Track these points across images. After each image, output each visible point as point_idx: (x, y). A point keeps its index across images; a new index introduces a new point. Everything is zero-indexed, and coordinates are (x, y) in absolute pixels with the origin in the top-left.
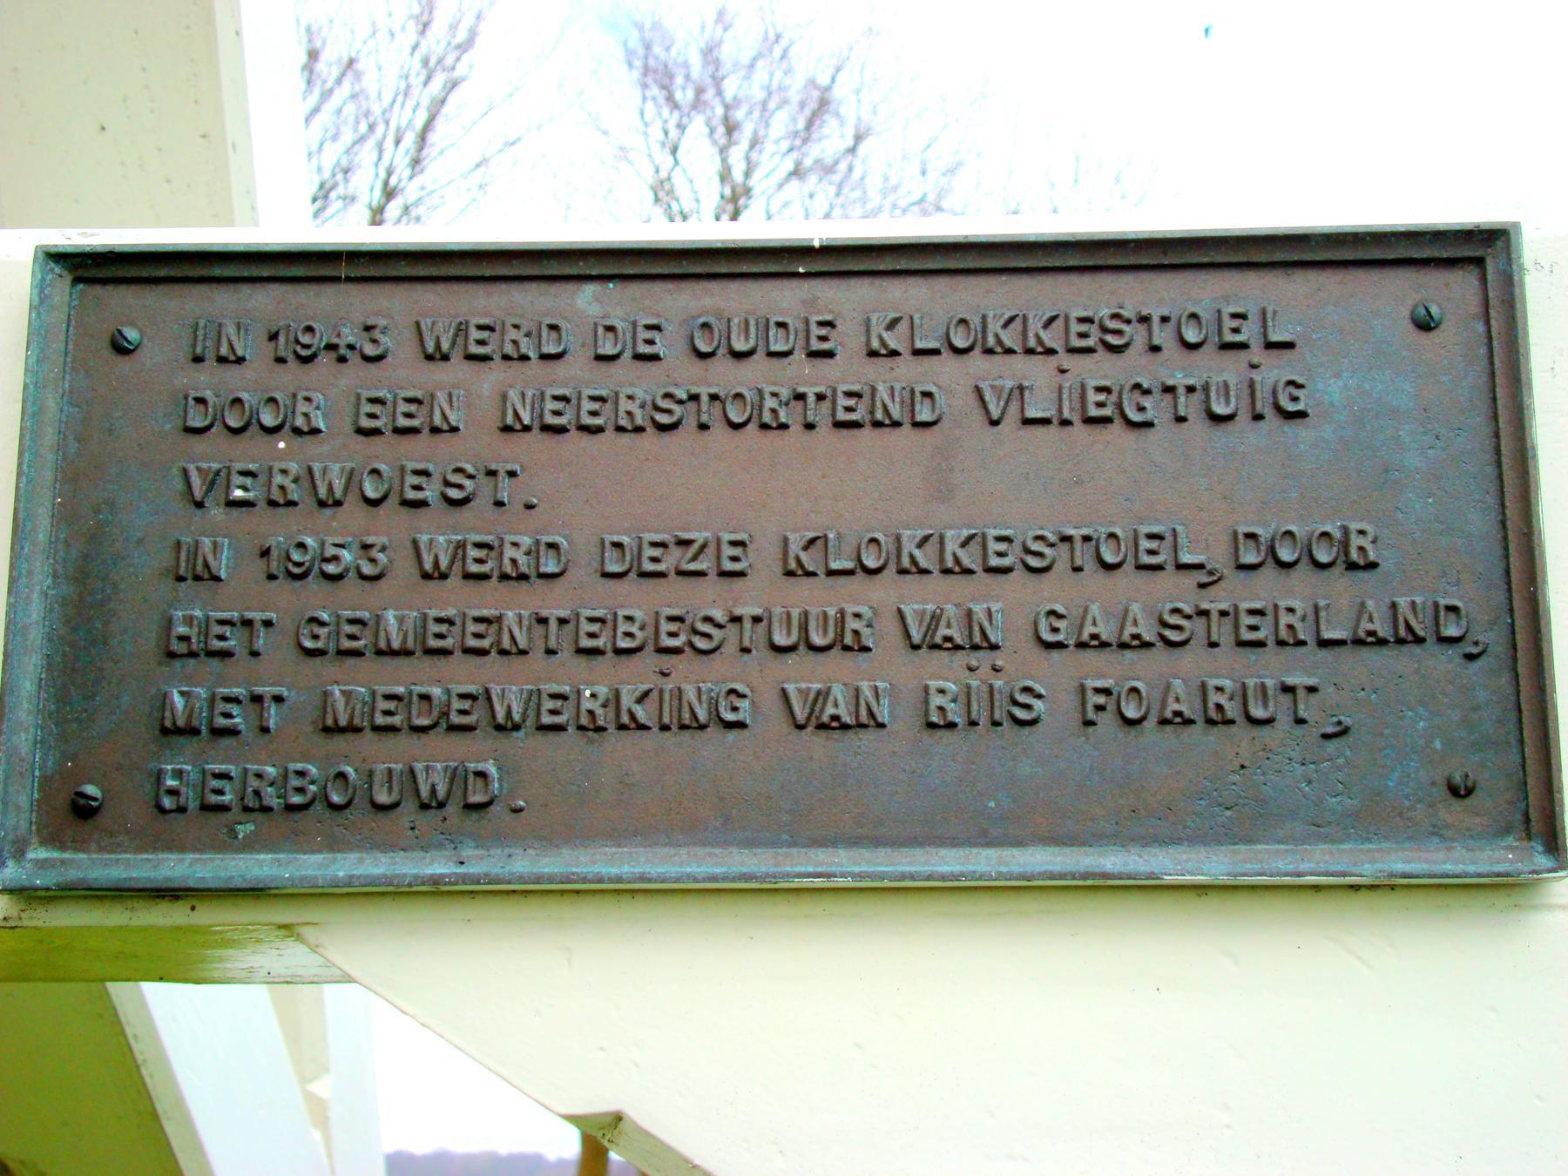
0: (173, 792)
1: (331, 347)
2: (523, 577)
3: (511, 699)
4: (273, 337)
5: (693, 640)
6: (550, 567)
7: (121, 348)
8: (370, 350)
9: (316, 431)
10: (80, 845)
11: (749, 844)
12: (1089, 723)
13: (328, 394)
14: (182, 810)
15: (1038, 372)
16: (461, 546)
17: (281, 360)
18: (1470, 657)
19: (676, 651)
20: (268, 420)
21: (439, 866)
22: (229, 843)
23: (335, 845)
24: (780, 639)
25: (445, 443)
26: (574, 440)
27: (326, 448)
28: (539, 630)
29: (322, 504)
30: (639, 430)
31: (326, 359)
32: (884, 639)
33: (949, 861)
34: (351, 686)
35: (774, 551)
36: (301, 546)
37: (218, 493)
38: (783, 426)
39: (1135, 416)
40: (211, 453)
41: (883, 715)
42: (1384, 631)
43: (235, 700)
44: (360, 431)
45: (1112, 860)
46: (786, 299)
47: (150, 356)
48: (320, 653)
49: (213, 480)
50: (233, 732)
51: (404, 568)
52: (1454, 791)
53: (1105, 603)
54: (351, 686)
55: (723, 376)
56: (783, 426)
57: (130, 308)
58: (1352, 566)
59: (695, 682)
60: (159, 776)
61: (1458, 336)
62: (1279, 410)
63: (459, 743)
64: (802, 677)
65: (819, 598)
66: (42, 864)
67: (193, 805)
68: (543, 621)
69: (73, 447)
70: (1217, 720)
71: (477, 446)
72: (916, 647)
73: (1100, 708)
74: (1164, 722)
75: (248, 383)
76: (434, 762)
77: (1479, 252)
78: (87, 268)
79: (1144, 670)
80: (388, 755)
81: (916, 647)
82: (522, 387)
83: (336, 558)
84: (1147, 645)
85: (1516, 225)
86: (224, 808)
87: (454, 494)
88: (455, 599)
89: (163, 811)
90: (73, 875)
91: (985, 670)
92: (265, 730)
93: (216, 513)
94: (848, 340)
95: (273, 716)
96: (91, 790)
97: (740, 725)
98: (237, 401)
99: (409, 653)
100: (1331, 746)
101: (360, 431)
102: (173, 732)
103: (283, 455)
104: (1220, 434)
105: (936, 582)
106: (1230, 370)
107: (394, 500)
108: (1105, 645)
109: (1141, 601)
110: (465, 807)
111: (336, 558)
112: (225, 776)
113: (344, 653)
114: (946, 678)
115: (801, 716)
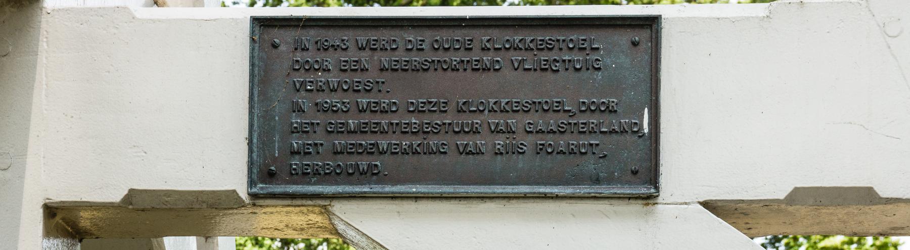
0: (295, 169)
1: (333, 46)
2: (387, 112)
3: (383, 143)
4: (317, 43)
5: (437, 130)
6: (394, 109)
7: (275, 46)
8: (344, 47)
9: (329, 70)
10: (270, 183)
11: (447, 185)
12: (538, 153)
13: (331, 59)
14: (297, 174)
15: (528, 55)
16: (369, 102)
17: (319, 50)
18: (640, 137)
19: (428, 132)
20: (316, 67)
21: (366, 189)
22: (309, 183)
23: (337, 183)
24: (457, 130)
25: (365, 74)
26: (400, 73)
27: (331, 75)
28: (390, 127)
29: (332, 91)
30: (418, 70)
31: (330, 49)
32: (484, 130)
33: (499, 189)
34: (340, 141)
35: (454, 104)
36: (326, 102)
37: (303, 87)
38: (458, 70)
39: (554, 68)
40: (298, 78)
41: (483, 150)
42: (554, 128)
43: (310, 145)
44: (341, 70)
45: (543, 189)
46: (459, 34)
47: (283, 48)
48: (531, 132)
49: (303, 83)
50: (310, 153)
51: (354, 109)
52: (632, 172)
53: (538, 120)
54: (340, 141)
55: (440, 56)
56: (458, 70)
57: (277, 36)
58: (610, 111)
59: (433, 141)
60: (291, 165)
61: (646, 45)
62: (593, 67)
63: (371, 157)
64: (462, 141)
65: (467, 119)
66: (262, 188)
67: (300, 173)
68: (392, 124)
69: (262, 73)
70: (572, 152)
71: (373, 75)
72: (493, 132)
73: (541, 149)
74: (558, 153)
75: (309, 57)
76: (363, 164)
77: (652, 23)
78: (260, 23)
79: (550, 140)
80: (352, 160)
81: (493, 132)
82: (385, 59)
83: (336, 106)
84: (555, 132)
85: (660, 16)
86: (309, 173)
87: (368, 88)
88: (366, 118)
89: (292, 174)
90: (270, 190)
91: (511, 139)
92: (318, 153)
93: (303, 93)
94: (476, 45)
95: (320, 149)
96: (273, 168)
97: (445, 153)
98: (308, 61)
99: (356, 132)
100: (601, 160)
101: (341, 70)
102: (294, 153)
103: (320, 77)
104: (577, 74)
105: (498, 114)
106: (577, 56)
107: (351, 90)
108: (544, 132)
109: (553, 120)
110: (371, 174)
111: (336, 106)
112: (308, 165)
113: (338, 132)
114: (500, 141)
115: (461, 150)
